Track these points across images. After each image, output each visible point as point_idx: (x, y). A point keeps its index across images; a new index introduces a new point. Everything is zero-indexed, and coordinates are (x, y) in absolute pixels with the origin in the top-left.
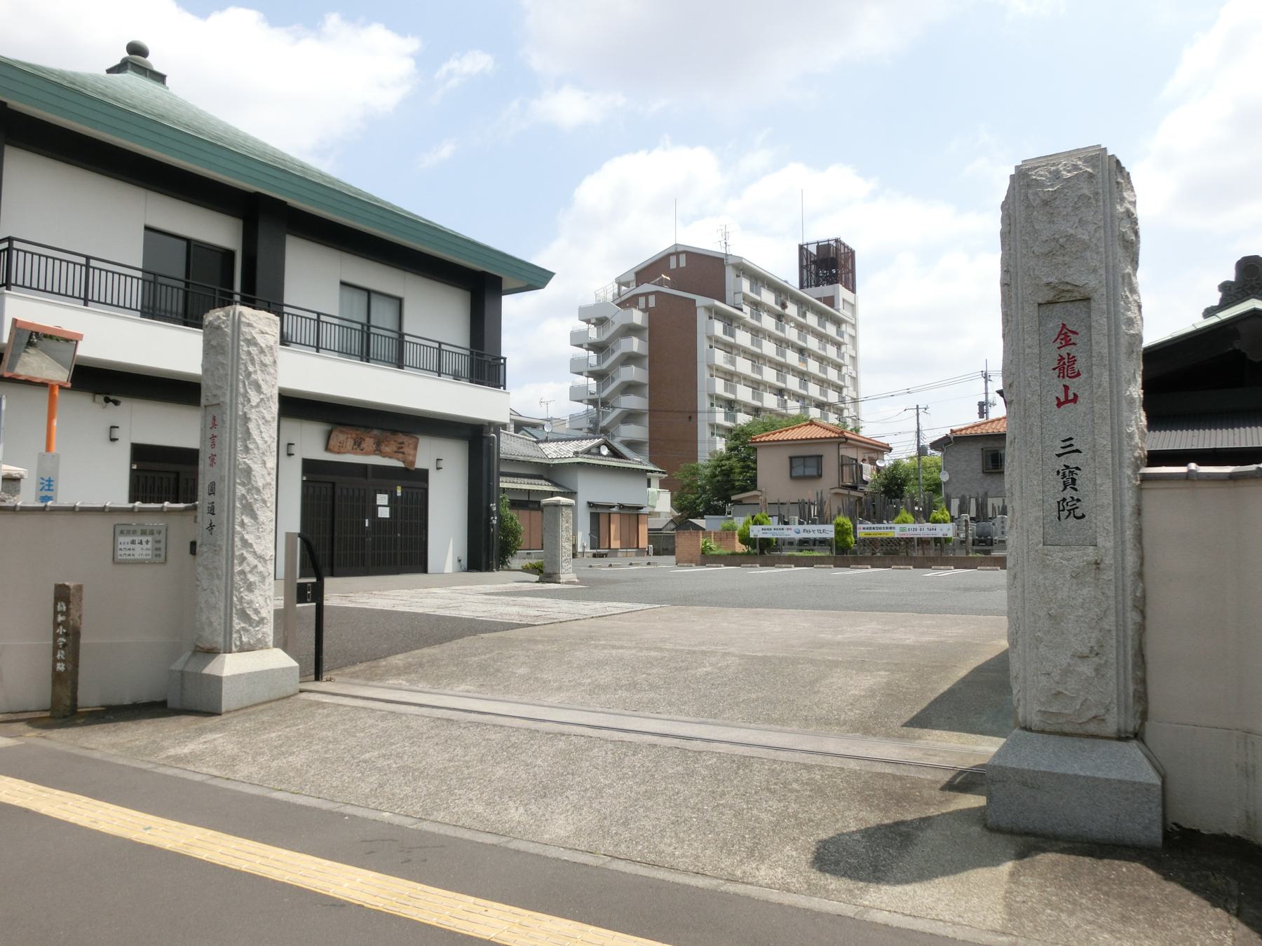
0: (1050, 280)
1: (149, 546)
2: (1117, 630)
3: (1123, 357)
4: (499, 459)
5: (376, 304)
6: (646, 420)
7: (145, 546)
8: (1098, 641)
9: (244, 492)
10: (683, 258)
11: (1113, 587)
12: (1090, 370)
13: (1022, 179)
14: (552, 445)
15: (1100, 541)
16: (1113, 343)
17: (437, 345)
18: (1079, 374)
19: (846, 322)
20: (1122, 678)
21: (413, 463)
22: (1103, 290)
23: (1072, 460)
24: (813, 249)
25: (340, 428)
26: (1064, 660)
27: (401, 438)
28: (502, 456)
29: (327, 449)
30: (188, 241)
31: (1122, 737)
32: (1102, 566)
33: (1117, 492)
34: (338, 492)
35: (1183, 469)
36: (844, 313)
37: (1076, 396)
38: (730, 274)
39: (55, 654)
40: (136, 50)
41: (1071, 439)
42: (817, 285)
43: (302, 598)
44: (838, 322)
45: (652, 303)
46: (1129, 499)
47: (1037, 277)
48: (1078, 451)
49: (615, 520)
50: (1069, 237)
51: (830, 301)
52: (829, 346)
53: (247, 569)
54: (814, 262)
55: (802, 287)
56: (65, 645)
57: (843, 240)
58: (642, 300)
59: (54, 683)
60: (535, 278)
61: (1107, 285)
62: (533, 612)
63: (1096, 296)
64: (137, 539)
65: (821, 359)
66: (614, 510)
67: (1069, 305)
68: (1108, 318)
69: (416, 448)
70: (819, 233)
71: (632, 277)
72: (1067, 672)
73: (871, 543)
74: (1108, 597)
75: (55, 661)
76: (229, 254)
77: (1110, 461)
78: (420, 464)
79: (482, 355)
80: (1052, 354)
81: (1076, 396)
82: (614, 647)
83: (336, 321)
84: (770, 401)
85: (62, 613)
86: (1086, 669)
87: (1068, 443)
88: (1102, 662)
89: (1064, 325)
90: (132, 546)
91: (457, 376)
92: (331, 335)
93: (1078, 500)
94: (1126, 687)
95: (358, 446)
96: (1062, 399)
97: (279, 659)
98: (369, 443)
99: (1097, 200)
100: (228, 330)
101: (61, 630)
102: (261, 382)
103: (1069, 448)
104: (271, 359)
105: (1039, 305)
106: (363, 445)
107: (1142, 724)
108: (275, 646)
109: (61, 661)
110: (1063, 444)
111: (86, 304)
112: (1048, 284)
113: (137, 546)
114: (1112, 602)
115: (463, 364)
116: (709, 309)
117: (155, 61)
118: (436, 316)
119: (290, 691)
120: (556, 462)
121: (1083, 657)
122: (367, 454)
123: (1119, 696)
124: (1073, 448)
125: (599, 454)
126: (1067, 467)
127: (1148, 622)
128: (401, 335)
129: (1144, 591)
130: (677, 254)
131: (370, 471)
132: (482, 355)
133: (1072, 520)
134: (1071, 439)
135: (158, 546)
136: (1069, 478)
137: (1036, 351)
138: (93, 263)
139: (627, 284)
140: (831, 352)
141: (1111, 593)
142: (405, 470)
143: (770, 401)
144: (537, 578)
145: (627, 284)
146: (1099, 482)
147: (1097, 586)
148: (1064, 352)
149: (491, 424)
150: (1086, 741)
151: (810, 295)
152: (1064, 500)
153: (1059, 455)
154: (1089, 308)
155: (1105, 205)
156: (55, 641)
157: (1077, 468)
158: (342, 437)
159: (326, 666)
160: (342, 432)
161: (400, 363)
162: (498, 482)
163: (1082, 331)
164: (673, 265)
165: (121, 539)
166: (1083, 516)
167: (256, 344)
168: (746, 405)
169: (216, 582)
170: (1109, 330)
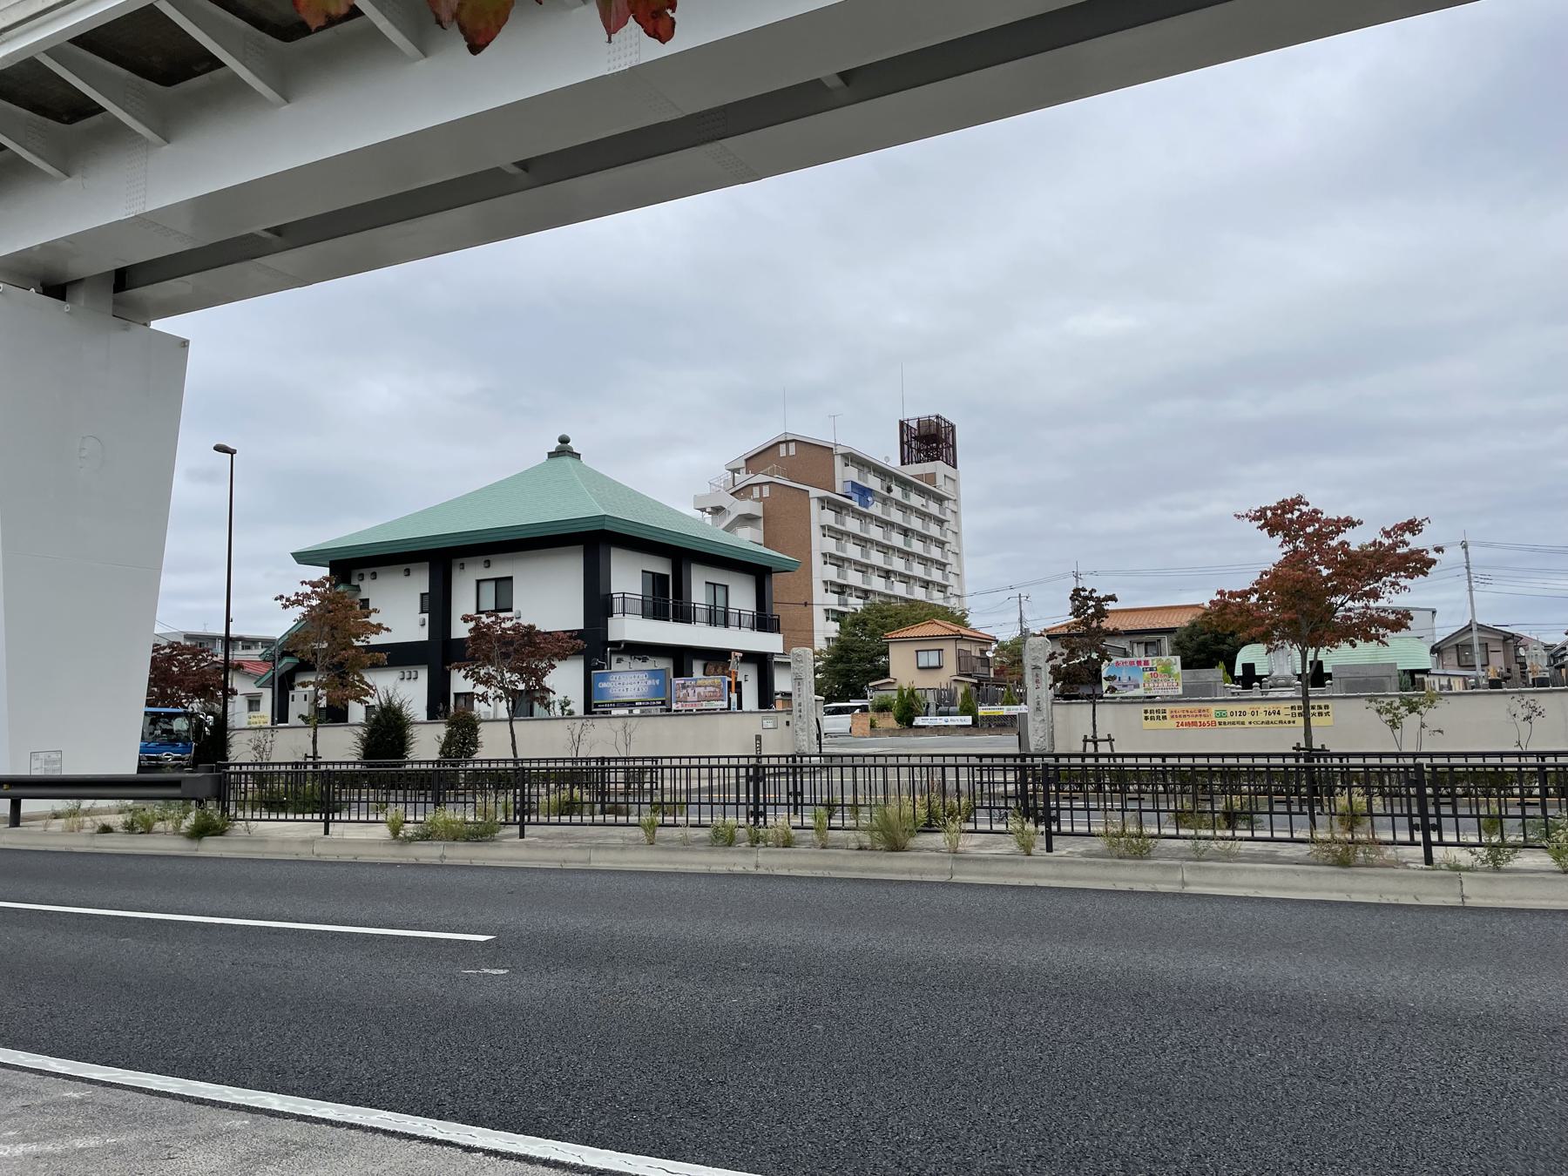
24: (914, 425)
36: (943, 488)
38: (838, 461)
40: (564, 440)
44: (940, 499)
45: (766, 493)
51: (931, 478)
52: (931, 503)
55: (903, 463)
58: (756, 490)
65: (924, 538)
70: (917, 412)
73: (989, 718)
84: (878, 584)
116: (821, 499)
130: (787, 442)
140: (934, 530)
143: (878, 584)
151: (911, 471)
164: (783, 453)
168: (857, 589)
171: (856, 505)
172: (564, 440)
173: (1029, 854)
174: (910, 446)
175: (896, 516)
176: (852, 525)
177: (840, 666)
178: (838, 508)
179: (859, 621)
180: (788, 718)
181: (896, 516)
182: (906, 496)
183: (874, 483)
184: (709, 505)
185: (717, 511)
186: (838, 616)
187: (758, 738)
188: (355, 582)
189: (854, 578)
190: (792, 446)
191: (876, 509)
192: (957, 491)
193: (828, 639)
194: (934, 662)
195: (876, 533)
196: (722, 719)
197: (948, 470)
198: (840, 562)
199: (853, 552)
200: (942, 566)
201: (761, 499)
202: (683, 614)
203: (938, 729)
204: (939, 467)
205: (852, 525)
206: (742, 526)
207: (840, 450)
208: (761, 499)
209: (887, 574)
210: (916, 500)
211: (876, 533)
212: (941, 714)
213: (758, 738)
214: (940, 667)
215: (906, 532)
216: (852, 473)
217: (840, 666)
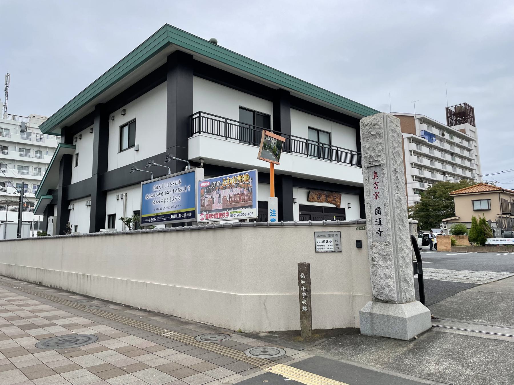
1: (332, 244)
7: (330, 244)
9: (399, 212)
19: (472, 140)
21: (340, 205)
24: (453, 109)
25: (312, 191)
27: (335, 195)
29: (308, 200)
30: (254, 112)
35: (321, 222)
36: (468, 134)
38: (417, 122)
42: (456, 125)
44: (468, 140)
51: (464, 131)
53: (405, 255)
54: (454, 115)
56: (306, 297)
57: (468, 103)
59: (302, 318)
62: (445, 275)
64: (326, 240)
65: (461, 157)
69: (340, 199)
70: (455, 101)
78: (342, 206)
85: (303, 279)
90: (323, 244)
95: (319, 200)
98: (323, 197)
100: (382, 125)
101: (303, 288)
106: (321, 198)
109: (304, 305)
111: (226, 139)
113: (326, 244)
116: (409, 139)
122: (322, 202)
135: (337, 243)
140: (466, 154)
142: (336, 208)
151: (456, 128)
156: (300, 294)
158: (313, 194)
160: (314, 193)
165: (318, 240)
167: (396, 132)
168: (429, 179)
169: (389, 262)
171: (427, 141)
174: (452, 119)
175: (447, 147)
176: (425, 150)
177: (423, 213)
178: (418, 142)
179: (431, 192)
180: (359, 235)
181: (447, 147)
182: (452, 138)
183: (435, 131)
186: (420, 192)
187: (304, 269)
188: (74, 144)
189: (427, 174)
191: (437, 143)
192: (476, 137)
193: (415, 202)
194: (485, 206)
195: (437, 154)
196: (248, 236)
197: (472, 128)
198: (420, 167)
199: (426, 162)
200: (471, 170)
203: (506, 248)
204: (467, 126)
205: (425, 150)
207: (418, 117)
209: (444, 173)
210: (456, 140)
211: (437, 154)
212: (506, 236)
213: (304, 269)
214: (489, 210)
215: (452, 154)
216: (425, 127)
217: (423, 213)
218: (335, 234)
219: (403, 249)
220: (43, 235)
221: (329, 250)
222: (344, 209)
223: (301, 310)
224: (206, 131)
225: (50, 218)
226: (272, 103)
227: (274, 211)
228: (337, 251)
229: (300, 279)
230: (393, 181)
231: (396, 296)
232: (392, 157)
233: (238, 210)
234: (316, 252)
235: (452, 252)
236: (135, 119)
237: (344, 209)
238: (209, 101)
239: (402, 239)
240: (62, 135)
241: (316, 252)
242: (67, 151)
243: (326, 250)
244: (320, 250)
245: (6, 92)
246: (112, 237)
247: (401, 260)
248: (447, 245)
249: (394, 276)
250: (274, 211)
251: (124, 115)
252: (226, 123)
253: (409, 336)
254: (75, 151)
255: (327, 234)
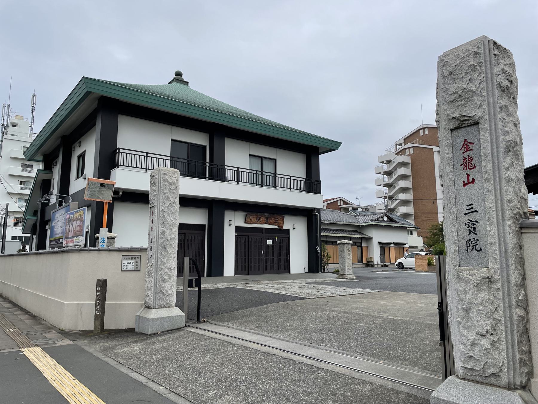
0: (455, 115)
1: (134, 264)
2: (505, 320)
3: (501, 155)
4: (321, 223)
5: (265, 163)
6: (412, 205)
7: (132, 264)
8: (492, 327)
10: (426, 130)
11: (501, 294)
12: (481, 165)
13: (443, 62)
14: (362, 217)
15: (491, 265)
16: (495, 147)
17: (289, 177)
18: (475, 167)
20: (510, 351)
21: (283, 227)
22: (487, 117)
23: (473, 217)
26: (472, 336)
27: (278, 217)
28: (322, 221)
31: (511, 387)
32: (492, 280)
33: (501, 235)
34: (250, 240)
37: (473, 179)
39: (96, 307)
40: (179, 74)
41: (472, 204)
43: (190, 286)
46: (511, 239)
47: (448, 115)
48: (476, 211)
49: (392, 251)
50: (464, 90)
56: (99, 304)
58: (407, 151)
59: (95, 319)
60: (332, 146)
61: (489, 114)
63: (481, 121)
64: (129, 262)
66: (392, 245)
67: (468, 128)
68: (491, 133)
69: (283, 221)
71: (403, 141)
72: (473, 344)
74: (498, 299)
75: (96, 310)
76: (205, 147)
77: (495, 216)
78: (285, 227)
79: (311, 181)
80: (460, 156)
81: (473, 179)
82: (330, 311)
83: (248, 171)
86: (485, 343)
87: (470, 207)
88: (496, 339)
89: (465, 140)
91: (301, 190)
92: (245, 177)
93: (478, 240)
94: (514, 356)
95: (258, 221)
96: (466, 182)
97: (177, 312)
99: (480, 67)
100: (157, 177)
101: (98, 298)
102: (170, 197)
103: (471, 210)
104: (175, 187)
105: (452, 130)
107: (528, 380)
108: (176, 306)
109: (98, 310)
110: (468, 208)
112: (454, 118)
113: (129, 265)
114: (501, 303)
115: (303, 185)
117: (184, 77)
118: (291, 167)
119: (181, 326)
120: (363, 224)
121: (483, 336)
122: (262, 224)
123: (508, 362)
124: (474, 210)
125: (383, 220)
126: (471, 221)
127: (531, 316)
128: (275, 174)
129: (526, 295)
130: (424, 129)
131: (264, 230)
132: (311, 181)
133: (474, 253)
134: (472, 204)
136: (472, 228)
137: (451, 156)
138: (149, 155)
139: (400, 145)
141: (500, 296)
144: (336, 276)
145: (400, 145)
146: (488, 229)
147: (490, 292)
148: (466, 155)
149: (315, 209)
150: (488, 387)
152: (470, 240)
153: (465, 214)
154: (479, 129)
155: (486, 67)
157: (476, 221)
158: (251, 217)
159: (202, 315)
161: (275, 187)
162: (320, 234)
163: (476, 143)
165: (124, 262)
166: (481, 250)
167: (168, 181)
169: (151, 279)
170: (491, 140)
172: (179, 74)
173: (477, 123)
184: (385, 160)
185: (389, 162)
187: (102, 284)
190: (426, 130)
201: (410, 155)
202: (218, 174)
206: (401, 167)
208: (410, 155)
213: (102, 284)
218: (136, 257)
219: (162, 269)
220: (22, 252)
221: (131, 269)
222: (288, 230)
223: (95, 313)
224: (127, 165)
225: (35, 237)
226: (208, 135)
227: (104, 239)
228: (137, 269)
229: (97, 291)
230: (160, 218)
231: (152, 303)
232: (162, 200)
233: (78, 238)
234: (122, 271)
235: (429, 272)
236: (85, 151)
237: (288, 230)
238: (131, 137)
239: (163, 261)
240: (42, 161)
241: (122, 271)
242: (46, 176)
243: (129, 269)
244: (125, 269)
245: (33, 112)
246: (12, 257)
247: (159, 277)
248: (424, 264)
249: (153, 288)
250: (104, 239)
251: (80, 146)
252: (147, 156)
253: (149, 333)
254: (52, 176)
255: (131, 257)
